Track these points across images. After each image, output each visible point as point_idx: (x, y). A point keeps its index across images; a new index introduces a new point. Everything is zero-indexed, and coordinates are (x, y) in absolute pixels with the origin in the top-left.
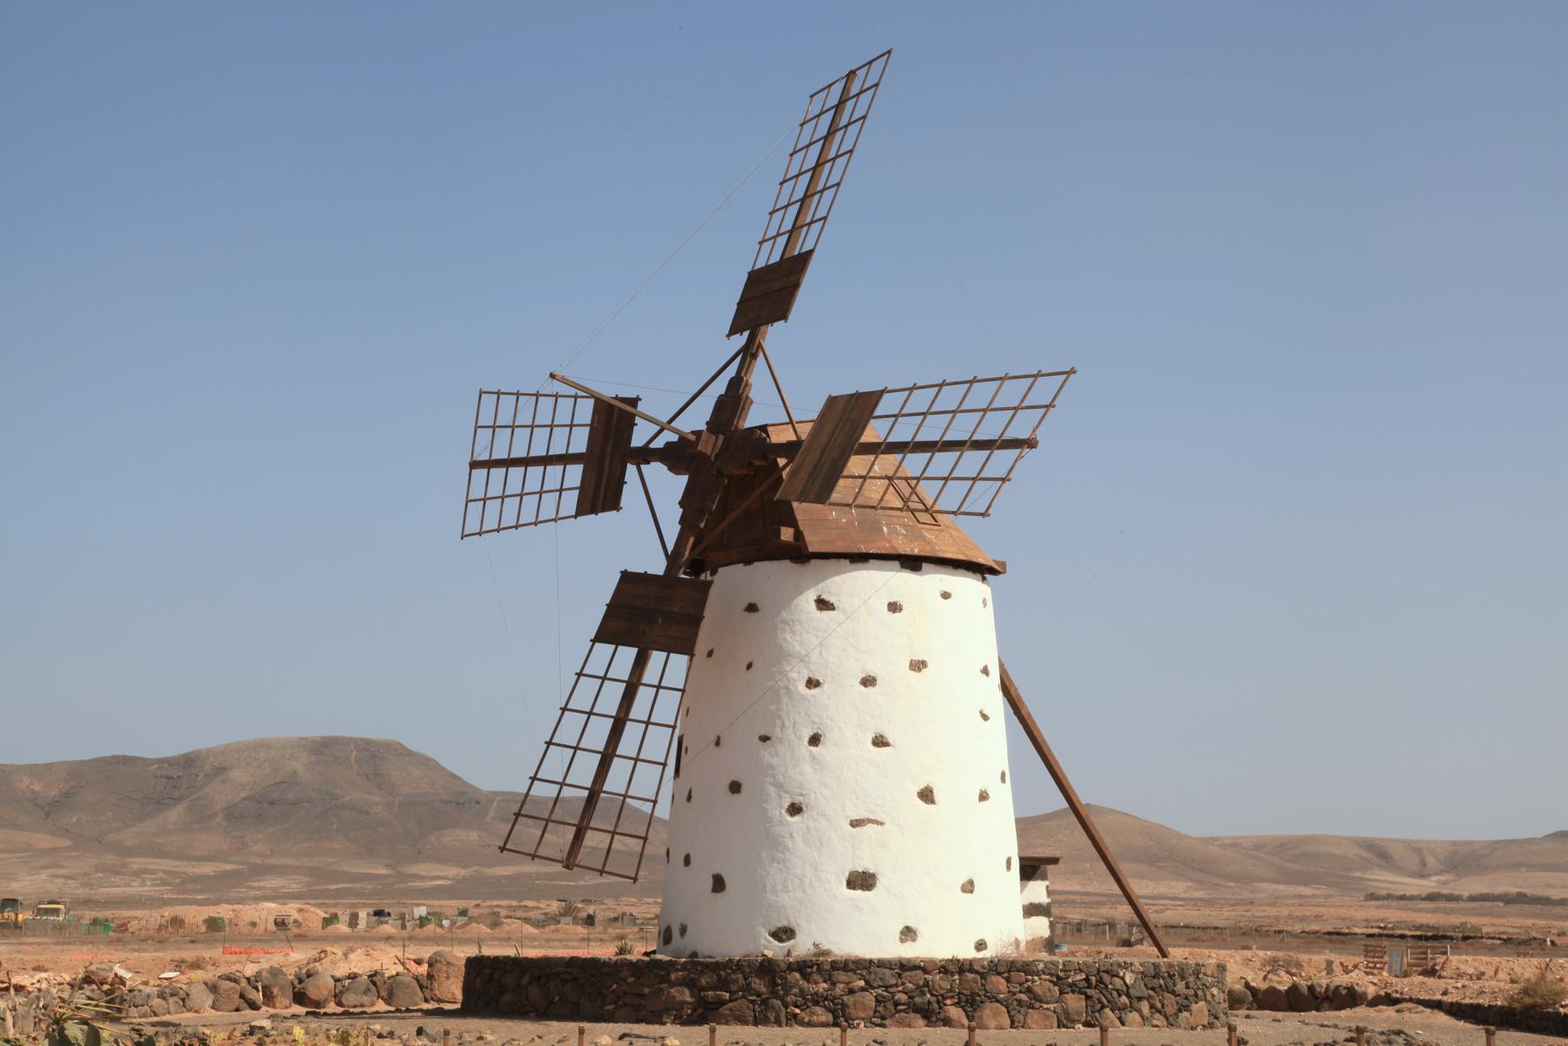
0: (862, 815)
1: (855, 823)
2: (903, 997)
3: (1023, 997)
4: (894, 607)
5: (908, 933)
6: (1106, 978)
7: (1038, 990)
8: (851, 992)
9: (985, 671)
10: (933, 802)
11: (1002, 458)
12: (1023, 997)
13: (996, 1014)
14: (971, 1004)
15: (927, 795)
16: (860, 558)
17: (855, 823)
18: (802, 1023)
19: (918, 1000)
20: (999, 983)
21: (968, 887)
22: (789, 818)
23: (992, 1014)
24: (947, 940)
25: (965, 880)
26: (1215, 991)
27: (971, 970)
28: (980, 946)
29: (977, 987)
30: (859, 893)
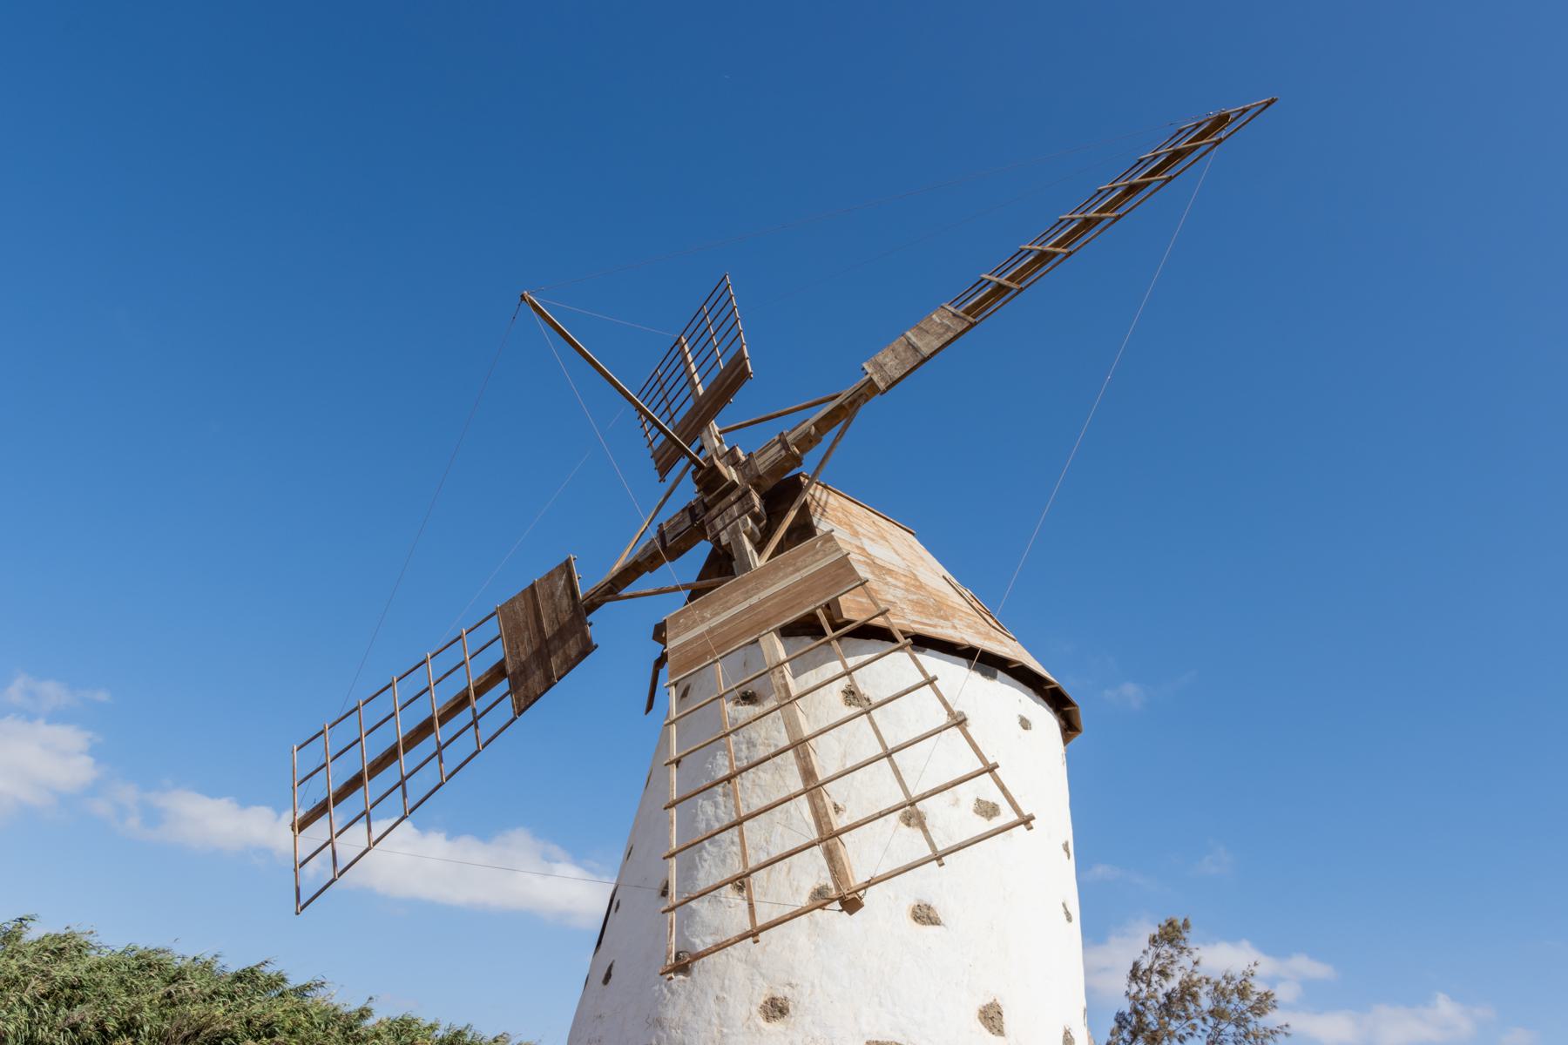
10: (1000, 1032)
15: (992, 1017)
22: (763, 1024)
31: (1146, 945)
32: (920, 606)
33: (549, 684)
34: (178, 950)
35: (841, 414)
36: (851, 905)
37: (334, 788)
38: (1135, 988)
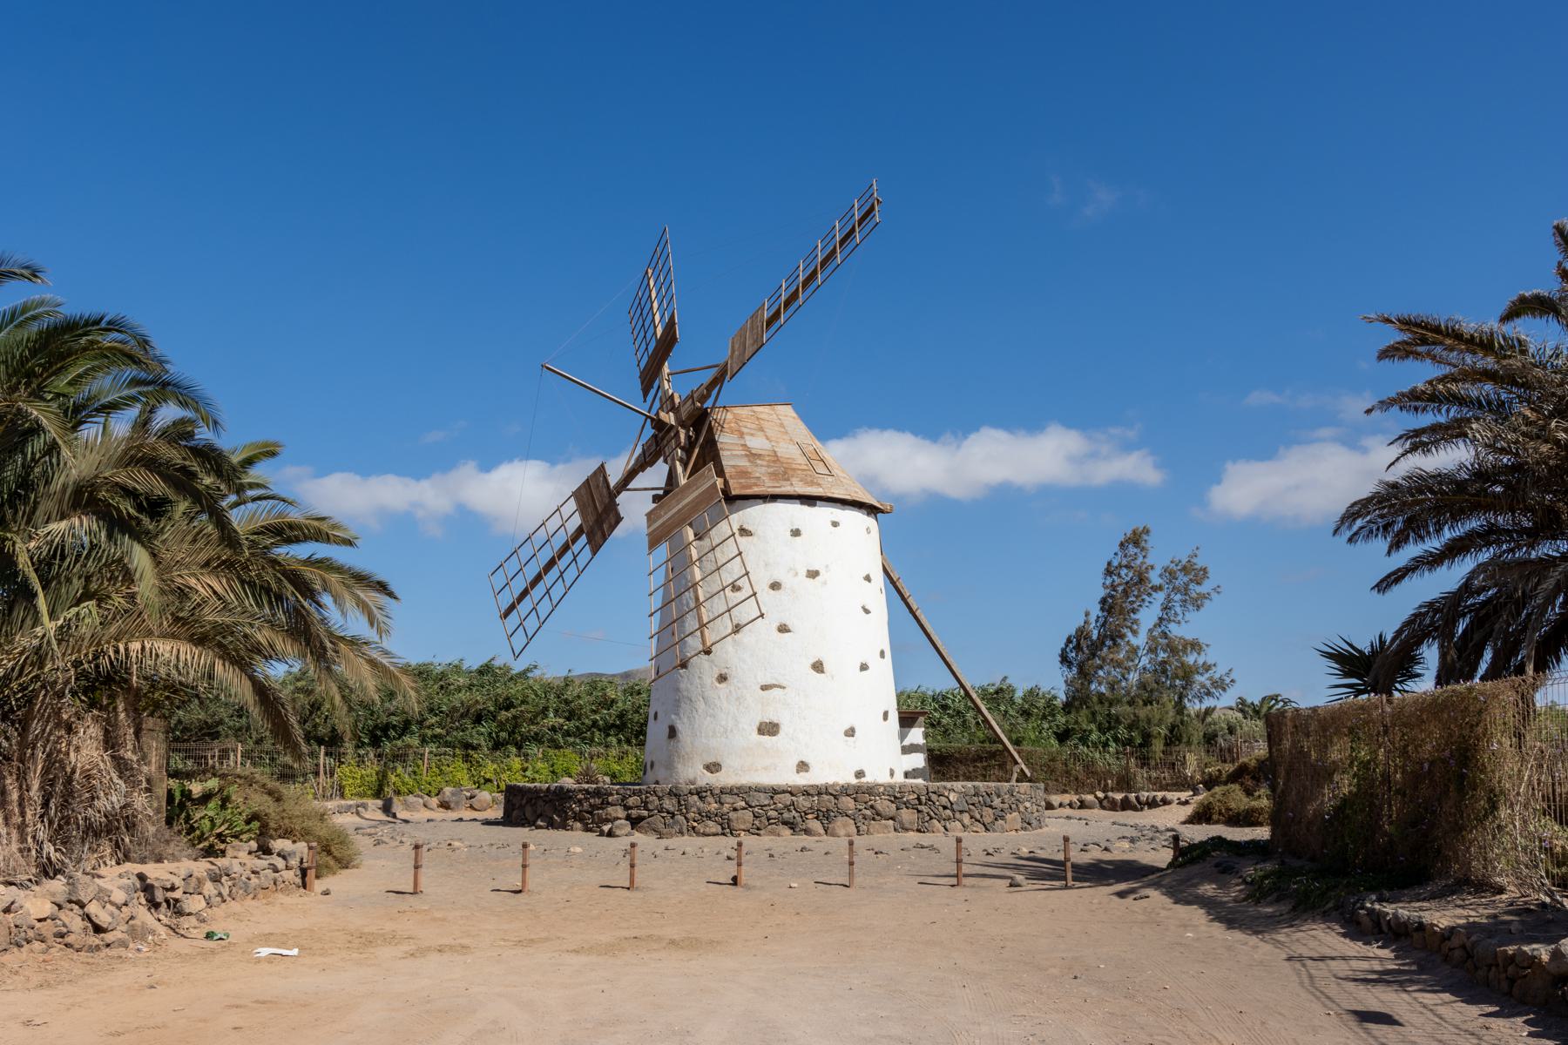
0: (769, 682)
1: (764, 688)
2: (773, 814)
3: (868, 812)
4: (796, 533)
5: (803, 766)
6: (934, 797)
7: (879, 807)
8: (735, 810)
9: (868, 578)
11: (506, 599)
12: (868, 812)
13: (845, 826)
14: (825, 816)
15: (818, 667)
16: (774, 498)
17: (764, 688)
18: (698, 834)
19: (786, 815)
20: (848, 803)
21: (850, 732)
23: (843, 826)
24: (832, 770)
25: (847, 727)
26: (1028, 804)
27: (827, 793)
28: (860, 774)
29: (831, 806)
30: (766, 738)
31: (1117, 549)
32: (774, 476)
33: (605, 539)
34: (436, 661)
35: (718, 381)
36: (708, 652)
37: (516, 595)
38: (1109, 581)
